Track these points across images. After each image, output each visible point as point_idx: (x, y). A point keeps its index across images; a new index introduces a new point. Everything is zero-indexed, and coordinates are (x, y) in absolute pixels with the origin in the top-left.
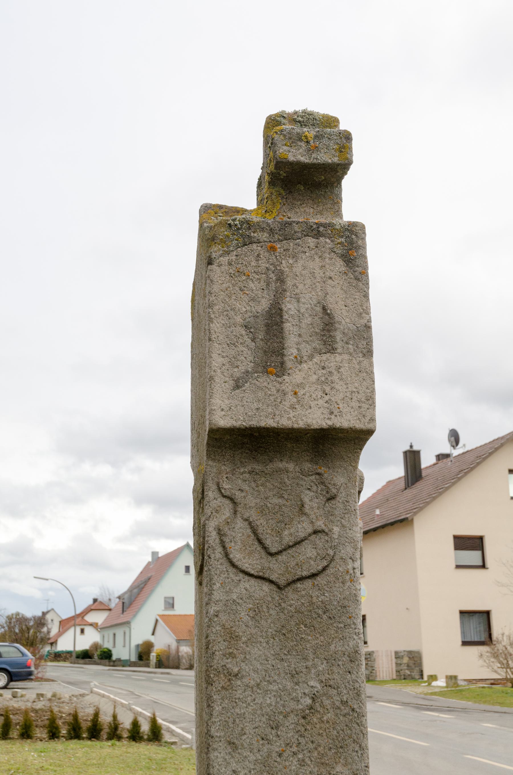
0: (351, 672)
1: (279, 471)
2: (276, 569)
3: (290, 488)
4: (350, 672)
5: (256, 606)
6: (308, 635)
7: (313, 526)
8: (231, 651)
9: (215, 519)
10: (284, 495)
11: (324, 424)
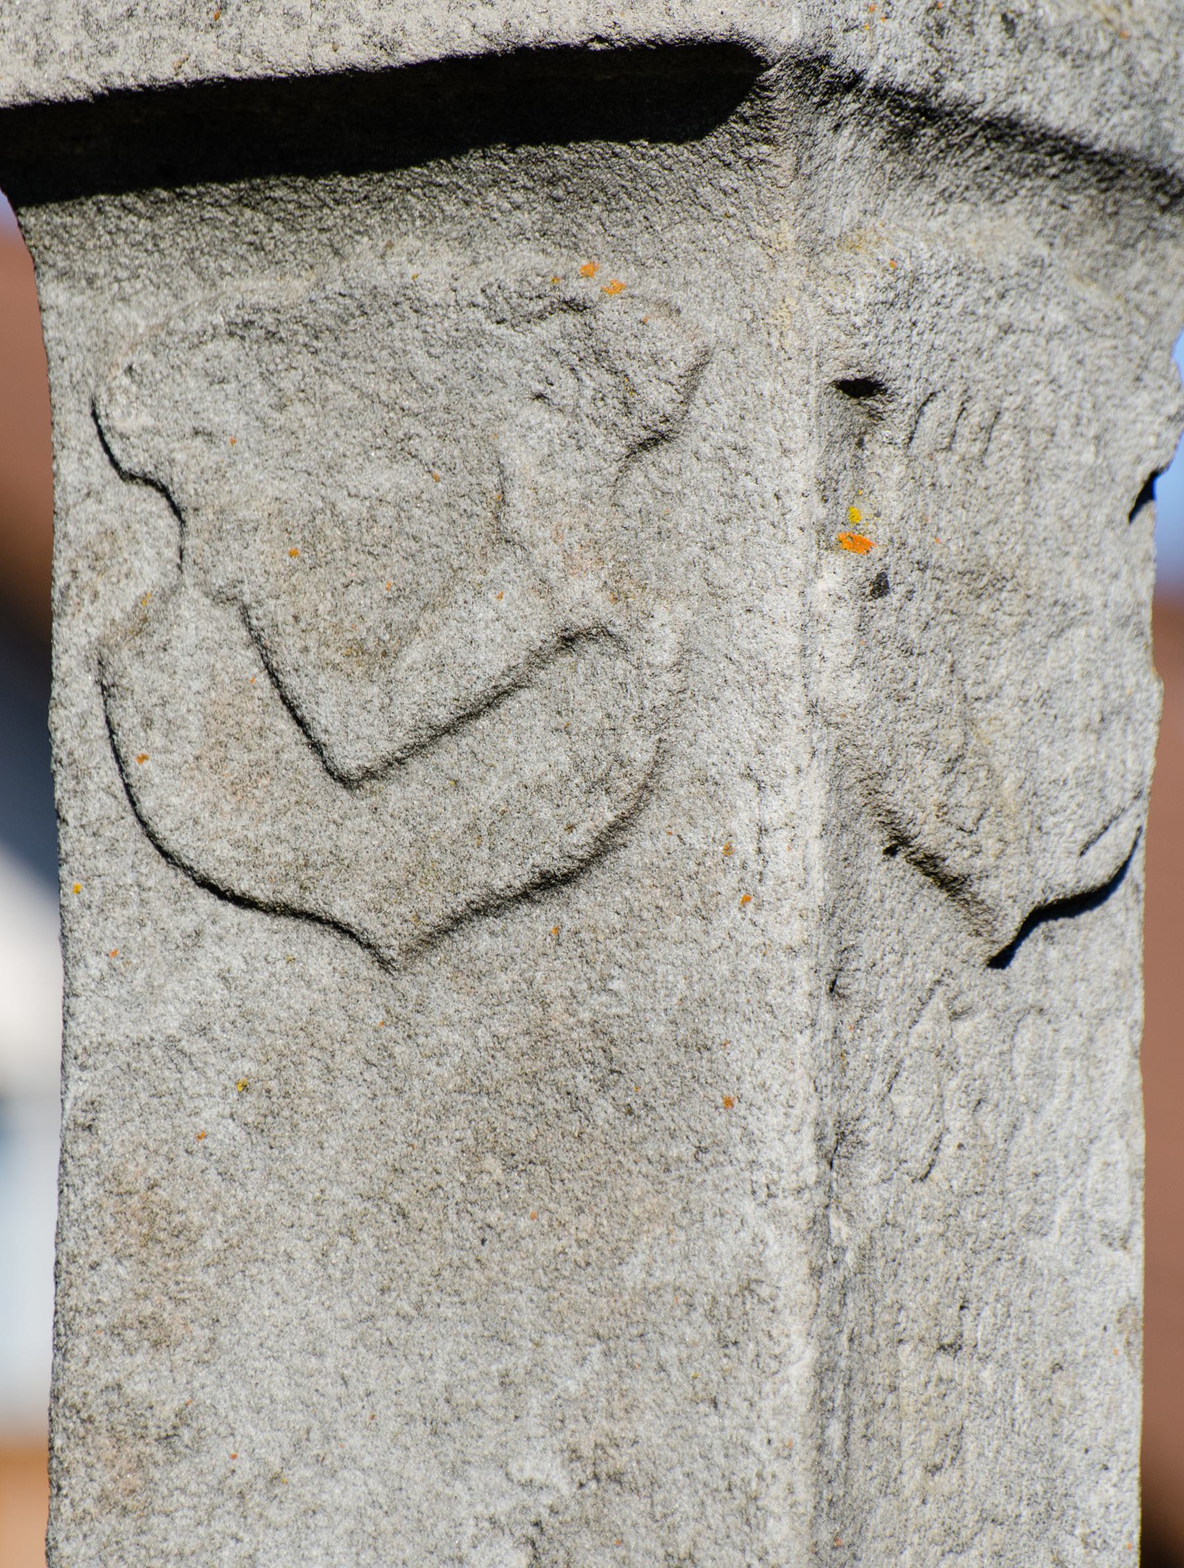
0: (721, 1399)
1: (367, 305)
2: (365, 854)
3: (442, 398)
4: (714, 1403)
5: (270, 1068)
6: (515, 1207)
7: (553, 605)
8: (147, 1309)
9: (88, 608)
10: (415, 442)
11: (465, 29)
